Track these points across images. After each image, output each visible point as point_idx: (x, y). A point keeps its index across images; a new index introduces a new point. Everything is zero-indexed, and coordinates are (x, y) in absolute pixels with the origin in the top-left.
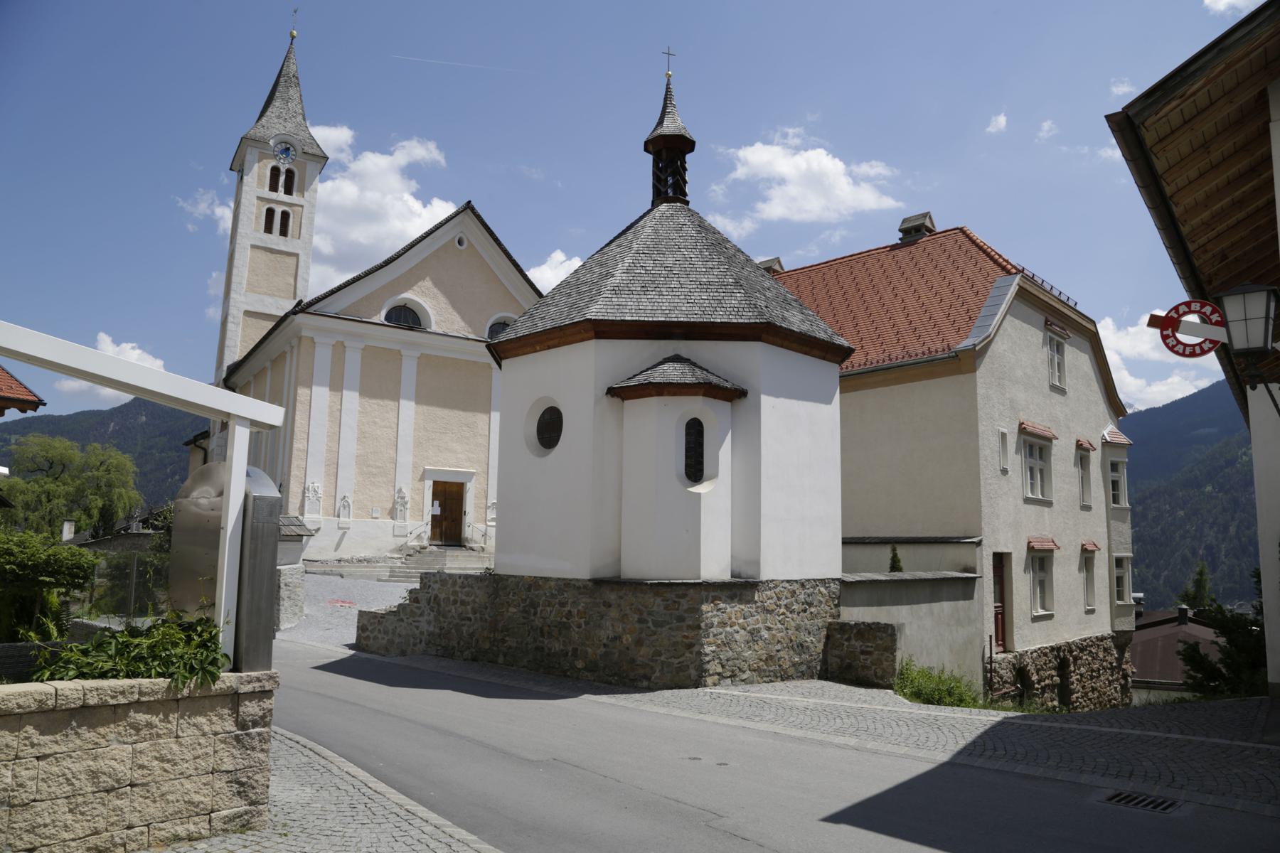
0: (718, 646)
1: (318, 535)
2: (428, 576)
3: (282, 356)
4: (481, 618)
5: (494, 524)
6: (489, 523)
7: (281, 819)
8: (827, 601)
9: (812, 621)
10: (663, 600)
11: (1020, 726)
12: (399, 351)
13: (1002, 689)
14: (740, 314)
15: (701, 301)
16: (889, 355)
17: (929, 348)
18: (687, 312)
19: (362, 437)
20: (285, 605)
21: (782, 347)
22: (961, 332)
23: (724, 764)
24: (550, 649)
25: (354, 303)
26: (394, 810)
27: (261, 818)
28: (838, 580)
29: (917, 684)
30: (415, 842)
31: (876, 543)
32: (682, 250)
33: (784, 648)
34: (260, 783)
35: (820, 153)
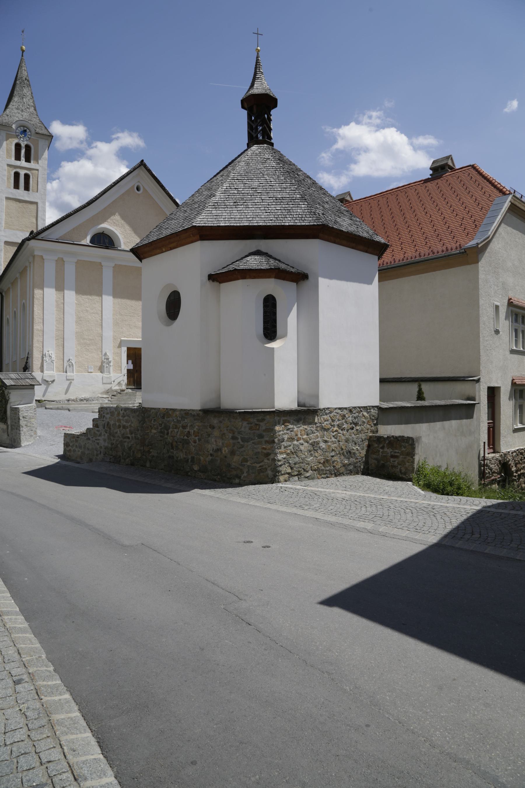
0: (288, 454)
2: (103, 409)
3: (25, 269)
4: (135, 437)
8: (368, 422)
9: (357, 435)
10: (248, 424)
11: (494, 514)
12: (100, 263)
13: (491, 477)
15: (276, 211)
16: (420, 253)
17: (447, 247)
18: (265, 219)
19: (79, 320)
20: (24, 430)
21: (334, 242)
24: (177, 458)
25: (68, 232)
28: (377, 407)
31: (409, 381)
32: (265, 176)
35: (393, 130)
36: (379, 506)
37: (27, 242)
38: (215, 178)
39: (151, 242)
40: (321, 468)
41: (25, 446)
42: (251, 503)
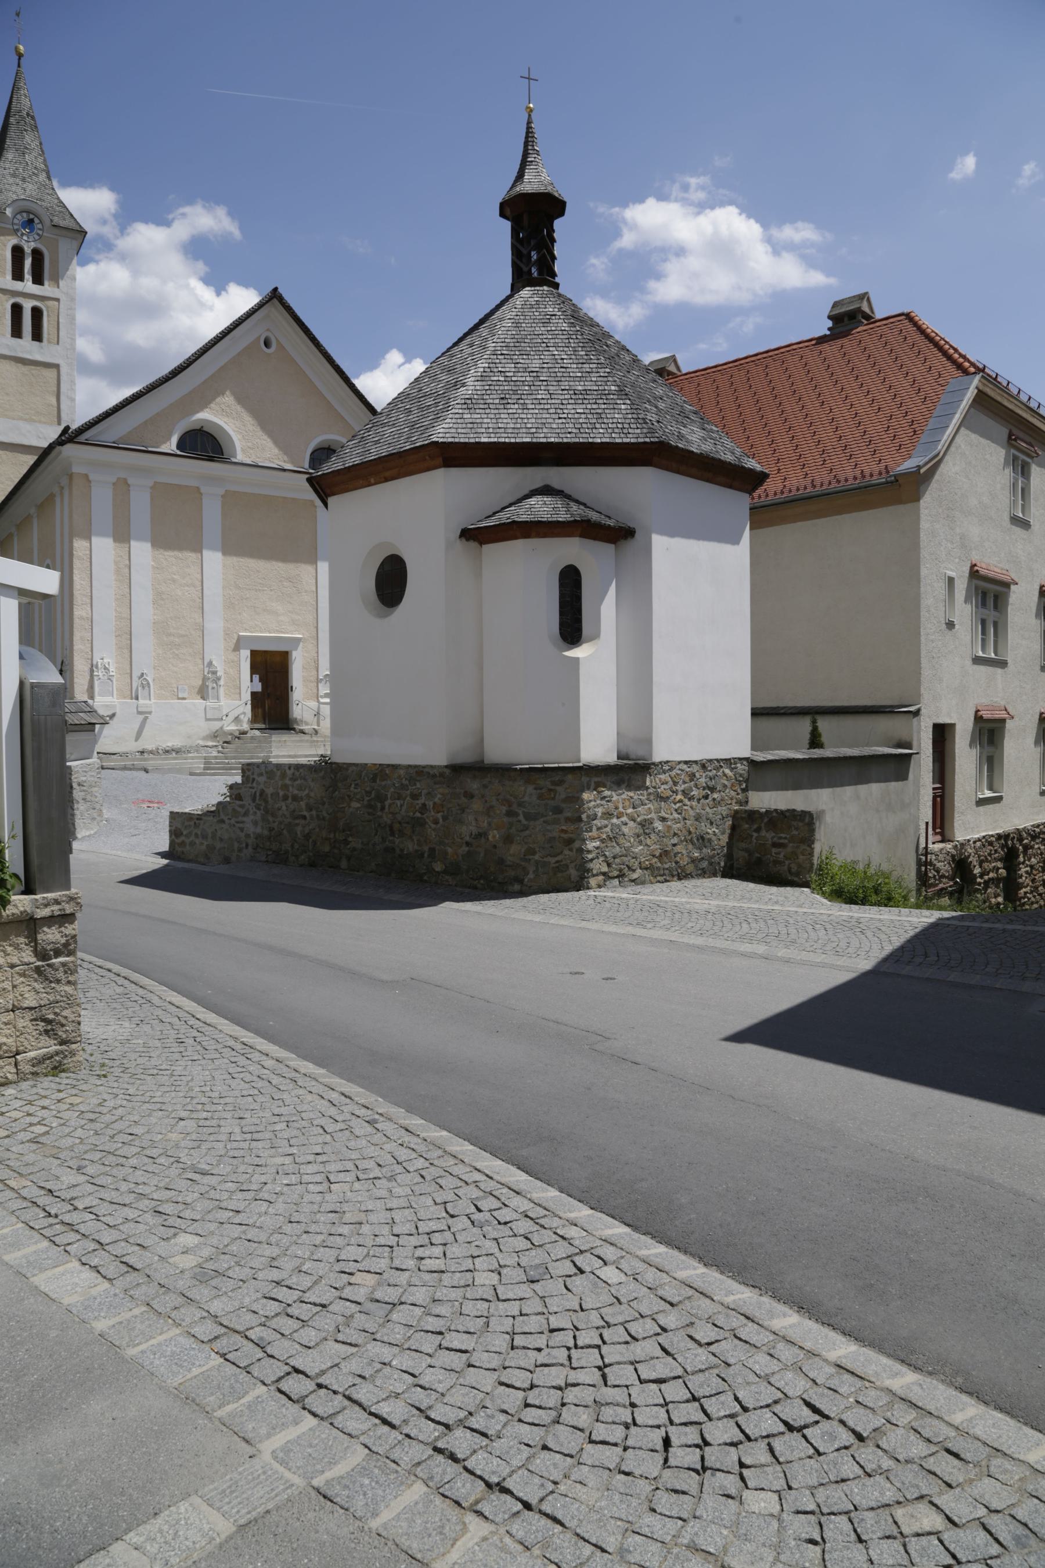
0: (603, 841)
1: (113, 723)
3: (51, 498)
4: (318, 816)
5: (328, 700)
6: (322, 700)
7: (98, 1058)
8: (732, 785)
10: (536, 789)
13: (938, 884)
14: (625, 431)
15: (576, 416)
18: (558, 431)
19: (159, 598)
21: (678, 472)
22: (903, 450)
23: (611, 979)
24: (402, 850)
25: (135, 428)
26: (228, 1044)
27: (74, 1059)
29: (838, 881)
30: (255, 1078)
32: (551, 349)
33: (682, 841)
34: (70, 1020)
35: (732, 210)
36: (769, 921)
37: (58, 448)
38: (456, 349)
39: (349, 467)
40: (655, 865)
41: (84, 837)
42: (552, 921)
